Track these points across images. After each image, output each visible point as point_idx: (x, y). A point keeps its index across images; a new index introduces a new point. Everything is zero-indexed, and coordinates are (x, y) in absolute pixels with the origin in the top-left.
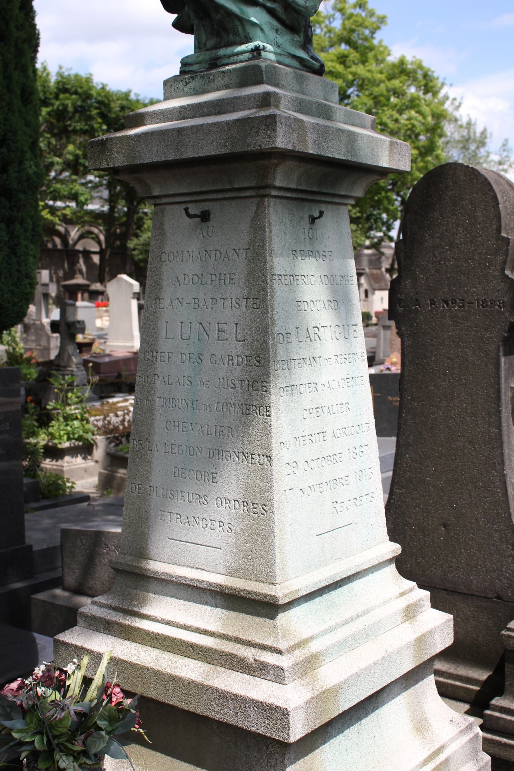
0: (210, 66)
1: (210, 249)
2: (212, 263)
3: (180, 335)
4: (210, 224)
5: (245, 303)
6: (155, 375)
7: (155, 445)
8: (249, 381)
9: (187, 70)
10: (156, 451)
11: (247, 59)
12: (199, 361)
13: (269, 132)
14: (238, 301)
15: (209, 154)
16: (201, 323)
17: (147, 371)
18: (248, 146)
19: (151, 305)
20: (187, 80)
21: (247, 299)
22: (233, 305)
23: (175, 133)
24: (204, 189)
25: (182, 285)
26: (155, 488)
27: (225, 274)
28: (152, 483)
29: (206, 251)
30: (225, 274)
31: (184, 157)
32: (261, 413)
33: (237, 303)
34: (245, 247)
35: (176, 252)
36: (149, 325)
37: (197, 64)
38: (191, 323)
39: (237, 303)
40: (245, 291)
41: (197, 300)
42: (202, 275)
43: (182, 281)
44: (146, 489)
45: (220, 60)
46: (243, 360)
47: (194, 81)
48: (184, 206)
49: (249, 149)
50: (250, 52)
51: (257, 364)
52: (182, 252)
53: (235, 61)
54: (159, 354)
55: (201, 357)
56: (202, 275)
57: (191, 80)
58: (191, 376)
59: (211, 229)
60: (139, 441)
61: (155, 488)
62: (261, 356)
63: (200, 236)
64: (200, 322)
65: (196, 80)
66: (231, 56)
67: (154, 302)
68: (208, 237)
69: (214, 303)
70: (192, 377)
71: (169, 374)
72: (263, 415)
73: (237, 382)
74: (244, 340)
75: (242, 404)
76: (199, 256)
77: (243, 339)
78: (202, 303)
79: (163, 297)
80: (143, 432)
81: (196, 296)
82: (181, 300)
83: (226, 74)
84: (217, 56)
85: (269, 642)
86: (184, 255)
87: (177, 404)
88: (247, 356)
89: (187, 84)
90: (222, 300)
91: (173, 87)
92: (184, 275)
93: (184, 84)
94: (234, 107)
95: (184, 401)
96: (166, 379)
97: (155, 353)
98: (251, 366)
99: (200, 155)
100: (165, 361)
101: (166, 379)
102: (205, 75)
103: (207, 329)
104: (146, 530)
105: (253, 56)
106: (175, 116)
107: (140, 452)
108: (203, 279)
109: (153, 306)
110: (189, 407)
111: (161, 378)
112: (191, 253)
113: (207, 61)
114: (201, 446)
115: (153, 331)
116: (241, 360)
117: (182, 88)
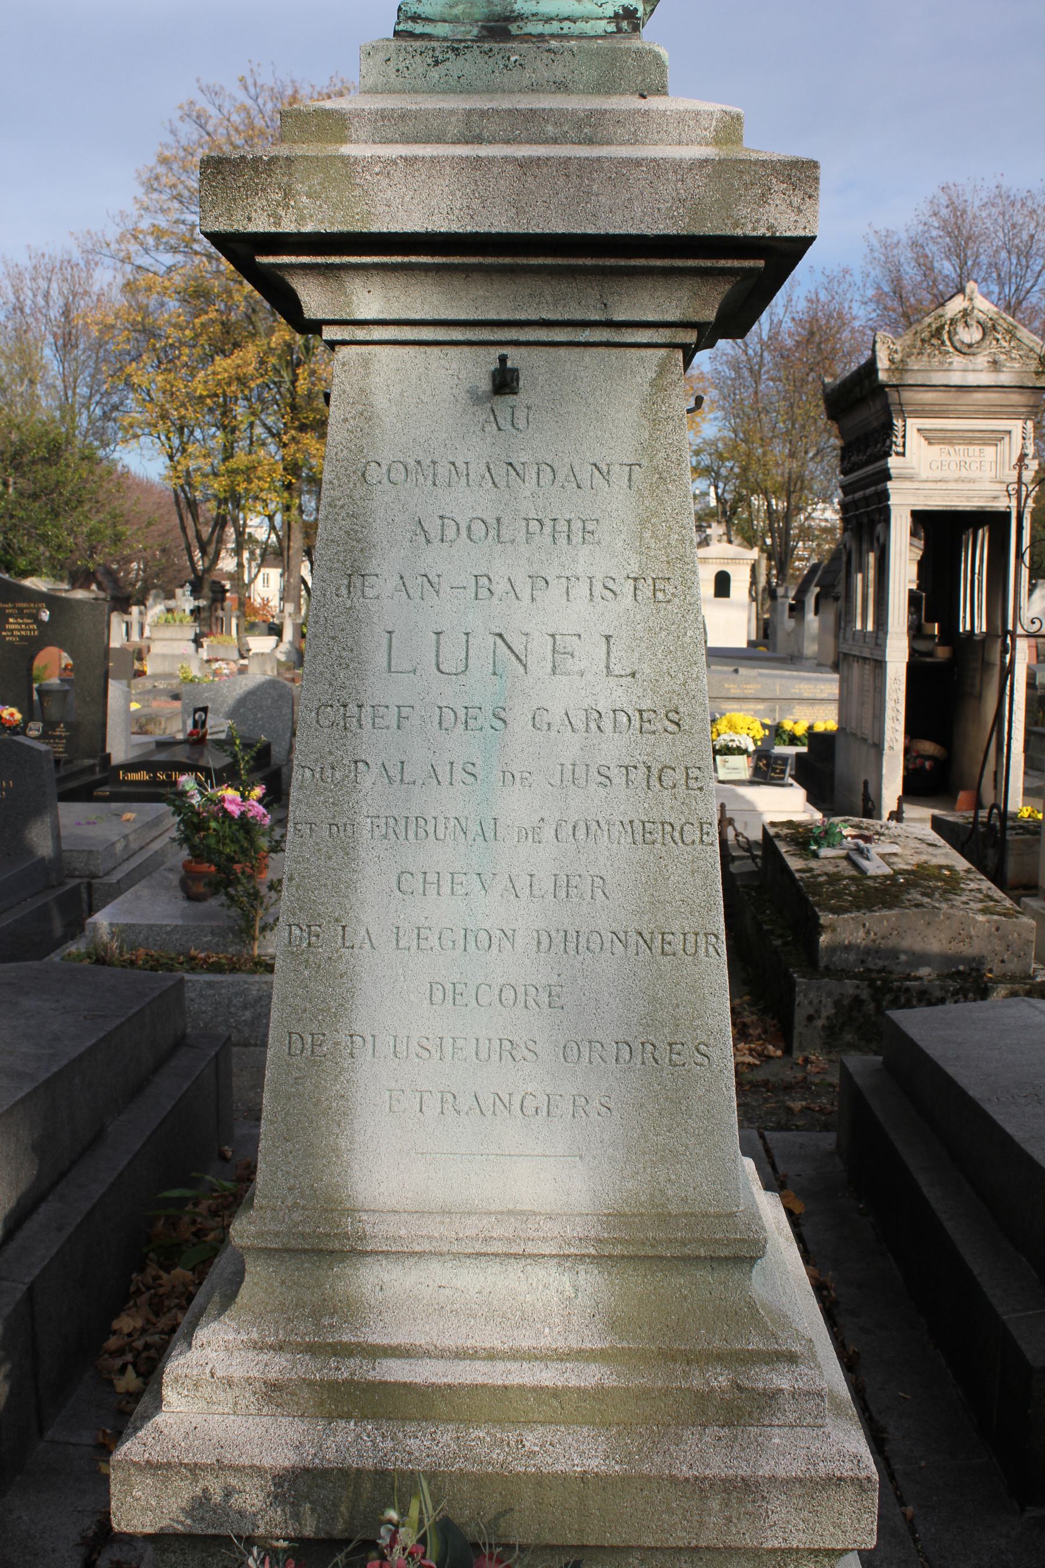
0: (485, 33)
1: (523, 460)
2: (528, 493)
3: (434, 662)
4: (519, 400)
5: (632, 588)
6: (356, 762)
7: (363, 932)
8: (649, 768)
9: (417, 32)
10: (367, 946)
11: (600, 32)
12: (499, 724)
13: (796, 201)
14: (610, 584)
15: (617, 231)
16: (500, 635)
17: (331, 753)
18: (736, 225)
19: (338, 589)
20: (437, 53)
21: (635, 579)
22: (596, 593)
23: (510, 168)
24: (522, 316)
25: (436, 542)
26: (369, 1038)
27: (569, 521)
28: (357, 1028)
29: (510, 464)
30: (569, 521)
31: (539, 231)
32: (688, 840)
33: (606, 588)
34: (626, 461)
35: (413, 463)
36: (333, 638)
37: (444, 21)
38: (467, 634)
39: (606, 588)
40: (632, 562)
41: (484, 581)
42: (498, 520)
43: (434, 533)
44: (337, 1044)
45: (521, 24)
46: (630, 720)
47: (462, 58)
48: (497, 352)
49: (739, 232)
50: (610, 18)
51: (672, 727)
52: (434, 463)
53: (565, 31)
54: (367, 710)
55: (503, 715)
56: (498, 520)
57: (450, 55)
58: (475, 761)
59: (521, 414)
60: (309, 926)
61: (369, 1038)
62: (681, 710)
63: (488, 429)
64: (497, 631)
65: (468, 56)
66: (552, 19)
67: (346, 582)
68: (514, 431)
69: (538, 586)
70: (479, 763)
71: (404, 758)
72: (693, 842)
73: (616, 771)
74: (633, 675)
75: (631, 822)
76: (487, 474)
77: (629, 671)
78: (501, 587)
79: (378, 571)
80: (322, 904)
81: (483, 570)
82: (435, 580)
83: (558, 57)
84: (513, 11)
85: (756, 1343)
86: (440, 470)
87: (431, 831)
88: (640, 711)
89: (437, 63)
90: (564, 580)
91: (391, 63)
92: (442, 517)
93: (430, 61)
94: (635, 133)
95: (453, 822)
96: (394, 772)
97: (352, 708)
98: (654, 732)
99: (591, 230)
100: (388, 728)
101: (394, 772)
102: (495, 51)
103: (518, 648)
104: (343, 1143)
105: (619, 30)
106: (453, 130)
107: (315, 955)
108: (503, 532)
109: (344, 591)
110: (471, 836)
111: (375, 769)
112: (462, 467)
113: (477, 21)
114: (513, 927)
115: (344, 654)
116: (625, 719)
117: (420, 70)
